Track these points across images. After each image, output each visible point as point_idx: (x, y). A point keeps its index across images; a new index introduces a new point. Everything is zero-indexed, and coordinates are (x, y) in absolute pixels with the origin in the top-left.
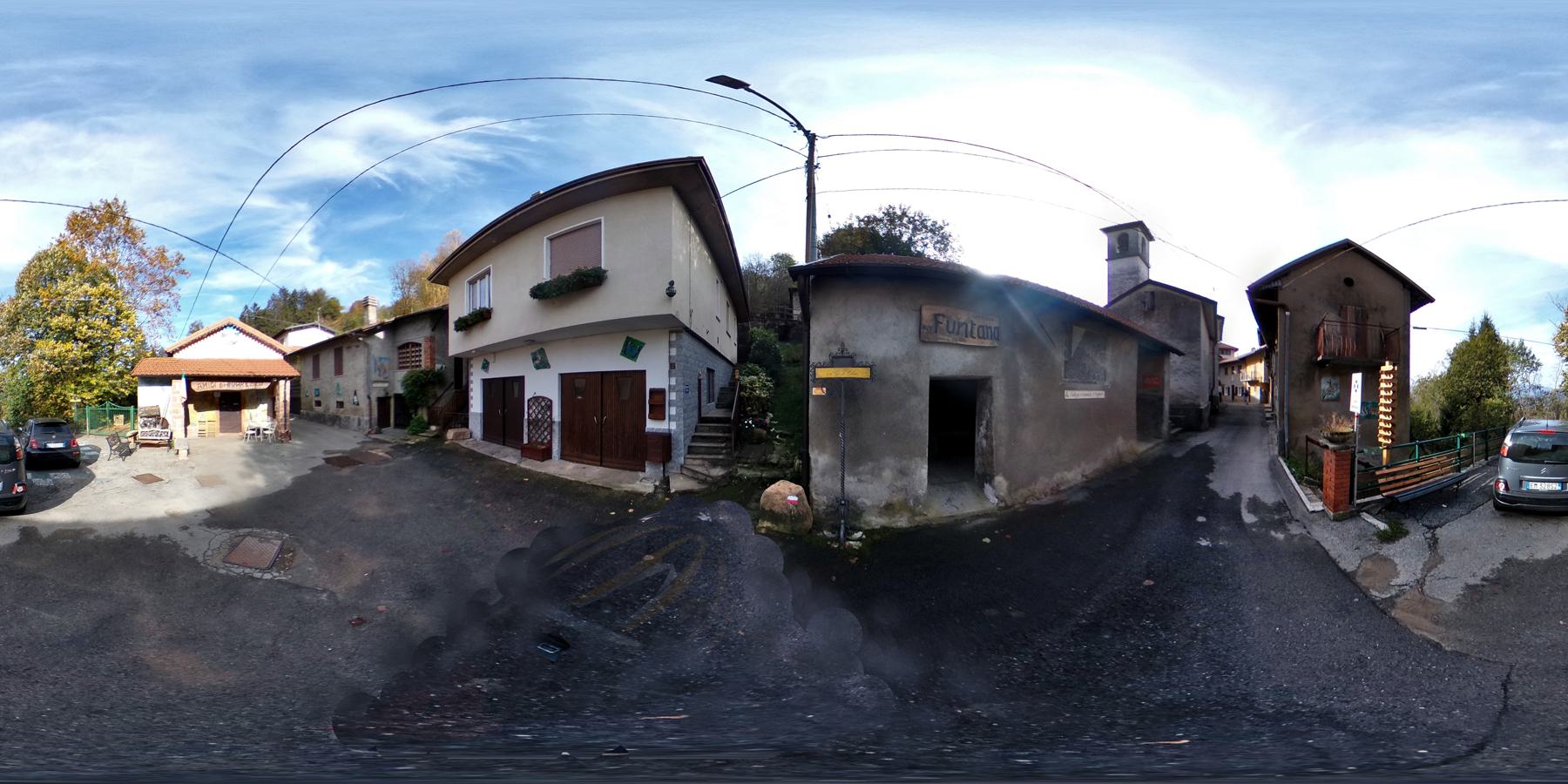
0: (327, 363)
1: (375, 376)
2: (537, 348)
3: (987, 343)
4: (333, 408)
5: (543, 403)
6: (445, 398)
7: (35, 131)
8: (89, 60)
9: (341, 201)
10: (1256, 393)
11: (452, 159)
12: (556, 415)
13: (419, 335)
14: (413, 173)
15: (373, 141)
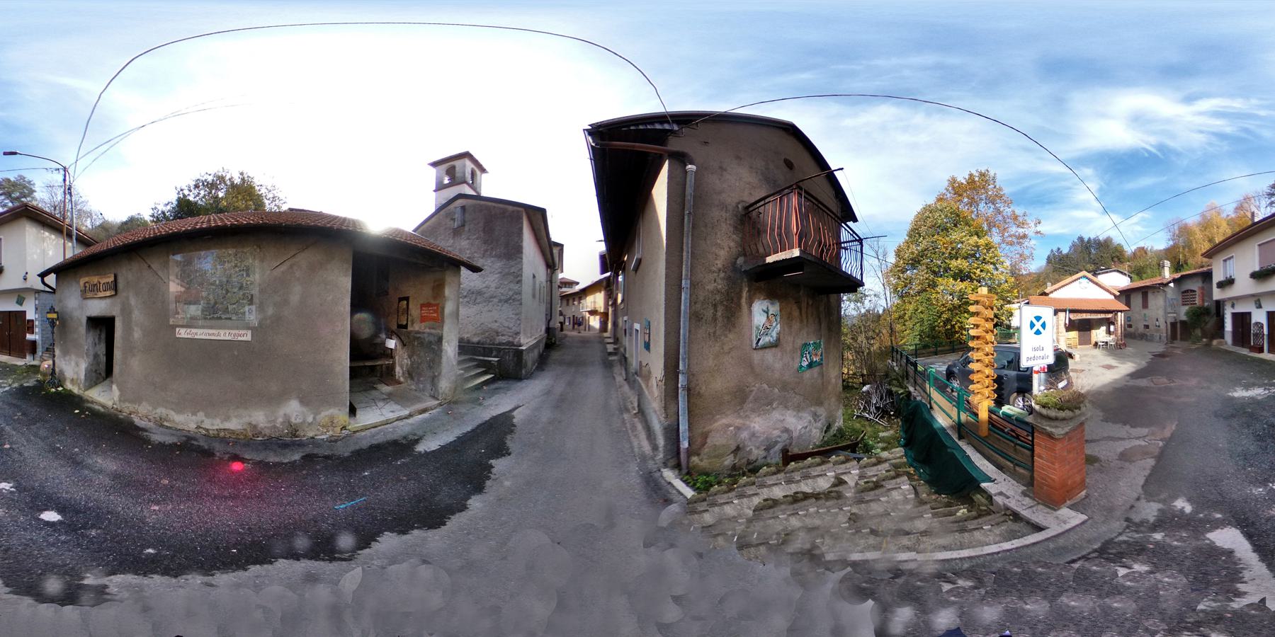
0: (1137, 300)
1: (1169, 310)
2: (1258, 300)
3: (108, 293)
4: (1141, 329)
5: (1259, 325)
6: (1211, 322)
7: (886, 111)
8: (929, 59)
9: (1119, 166)
10: (595, 322)
11: (1201, 132)
12: (1266, 331)
13: (1195, 285)
14: (1171, 143)
15: (1138, 120)
